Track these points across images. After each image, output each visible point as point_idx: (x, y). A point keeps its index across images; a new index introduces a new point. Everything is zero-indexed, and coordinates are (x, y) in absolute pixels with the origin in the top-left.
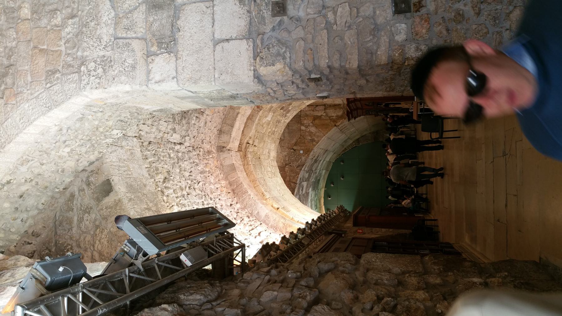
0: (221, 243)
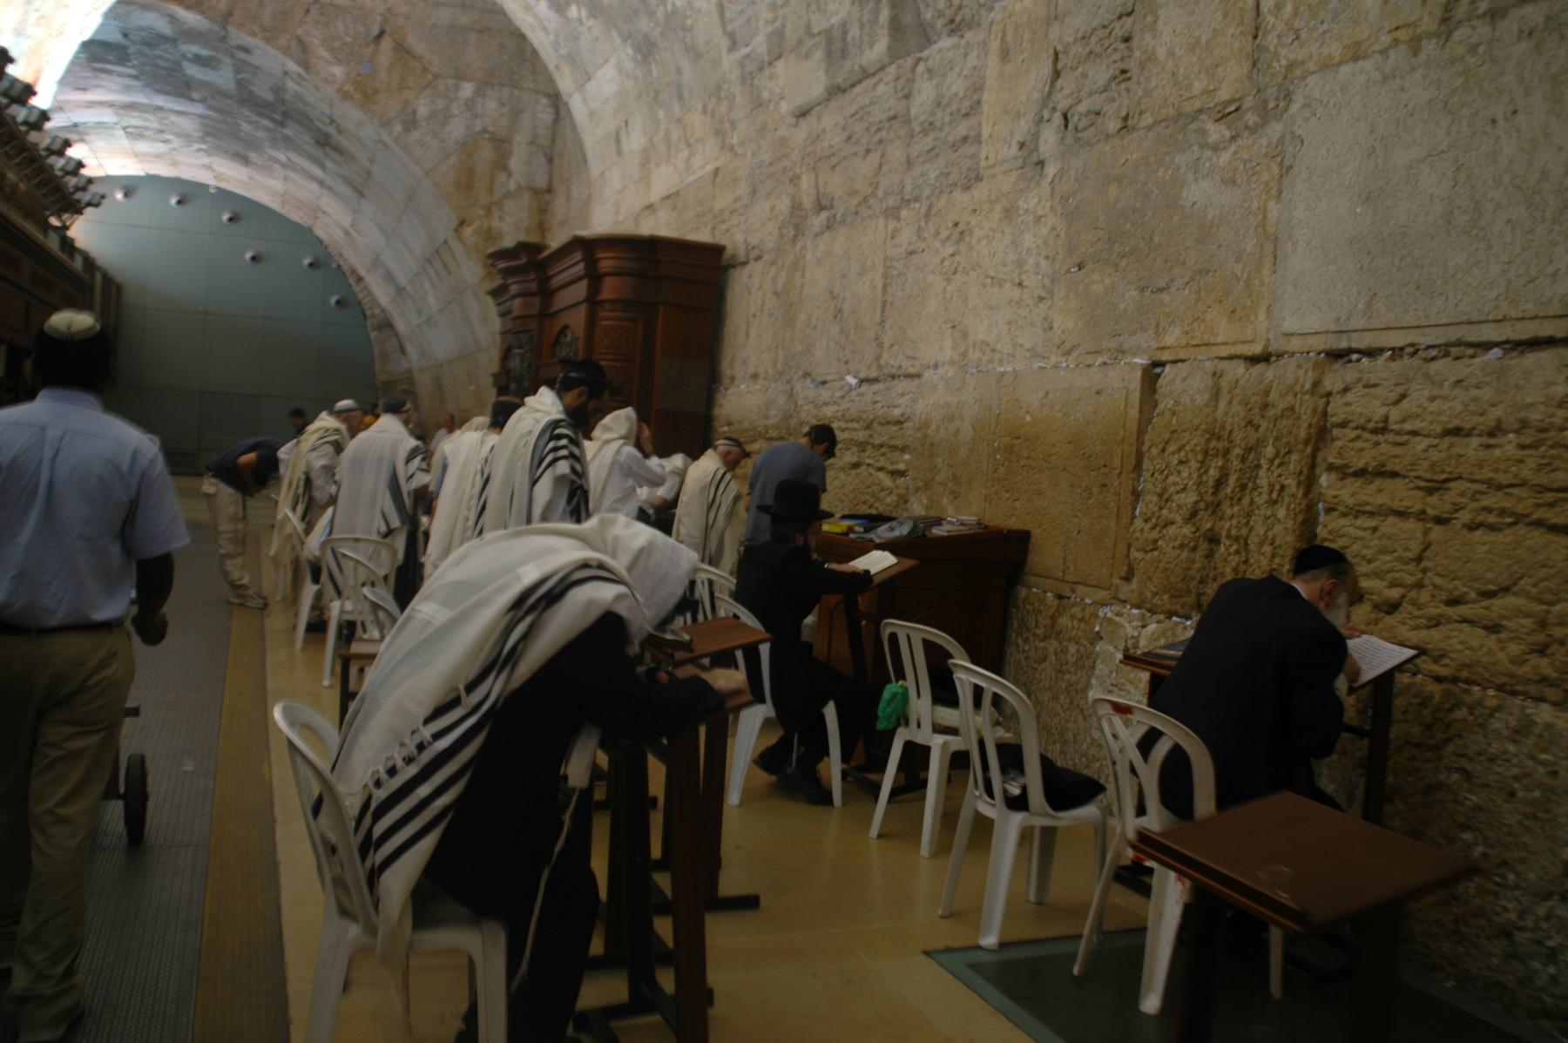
0: (92, 105)
